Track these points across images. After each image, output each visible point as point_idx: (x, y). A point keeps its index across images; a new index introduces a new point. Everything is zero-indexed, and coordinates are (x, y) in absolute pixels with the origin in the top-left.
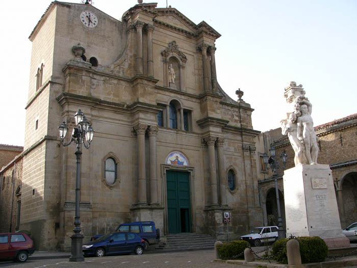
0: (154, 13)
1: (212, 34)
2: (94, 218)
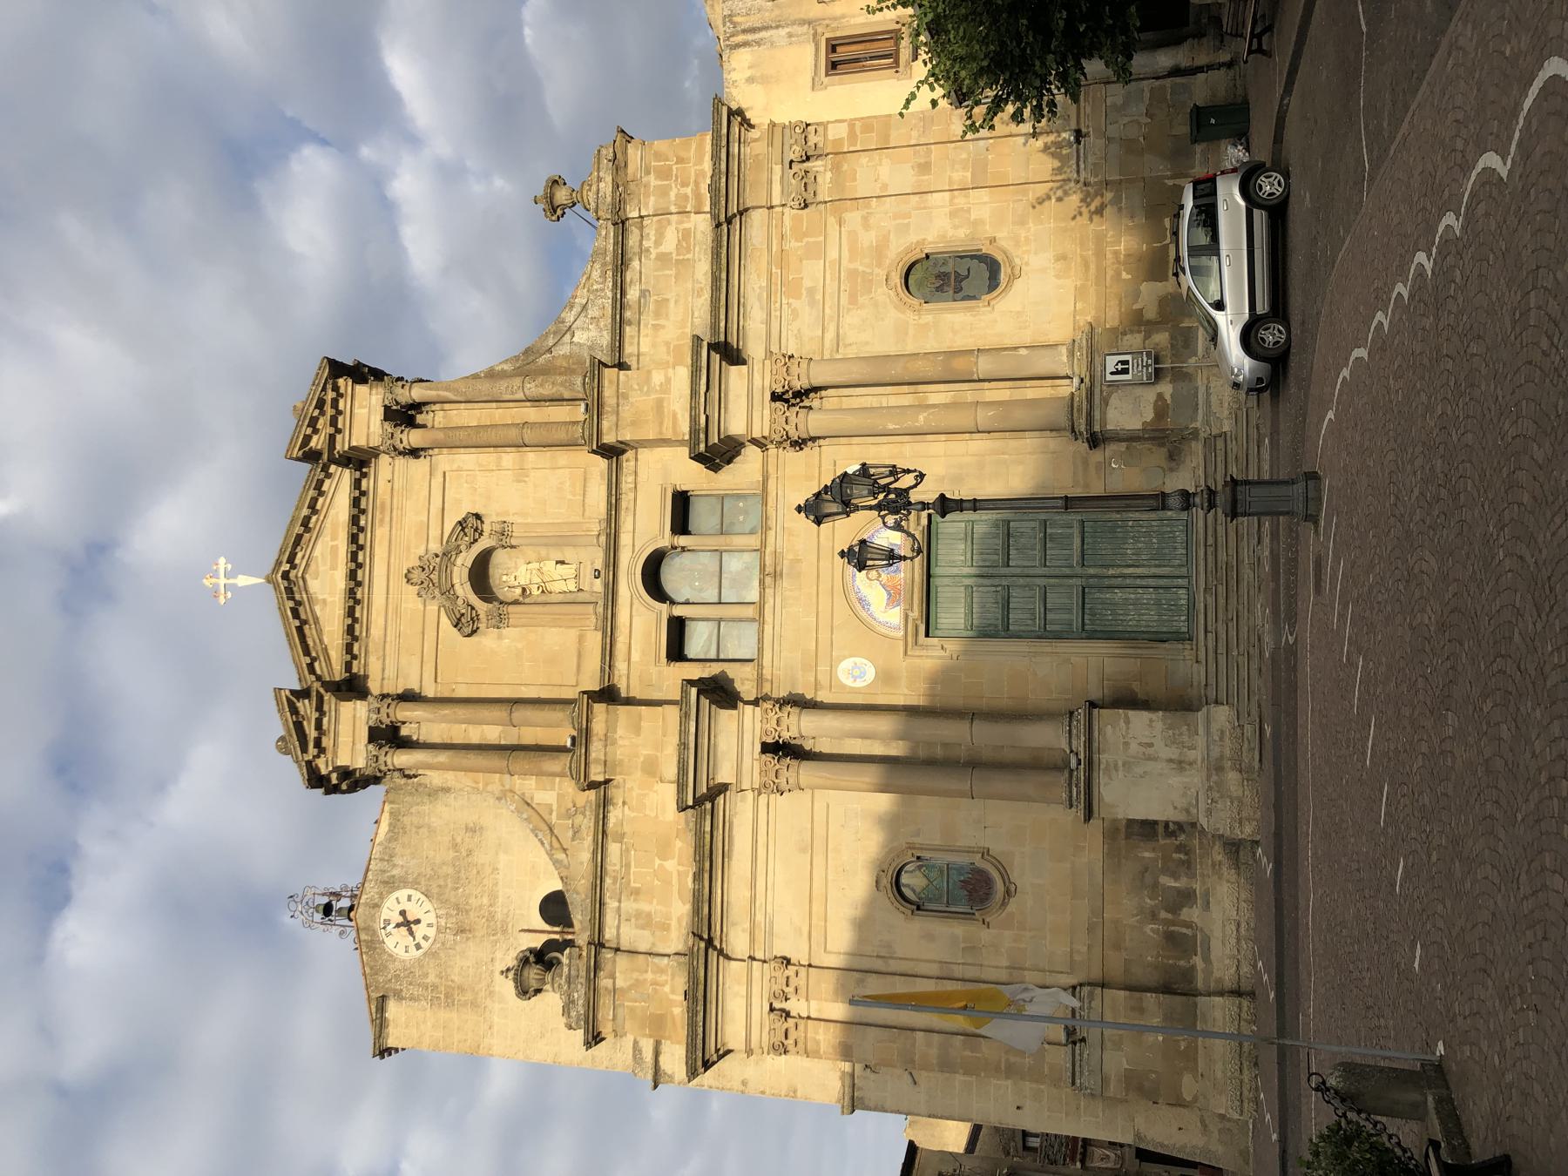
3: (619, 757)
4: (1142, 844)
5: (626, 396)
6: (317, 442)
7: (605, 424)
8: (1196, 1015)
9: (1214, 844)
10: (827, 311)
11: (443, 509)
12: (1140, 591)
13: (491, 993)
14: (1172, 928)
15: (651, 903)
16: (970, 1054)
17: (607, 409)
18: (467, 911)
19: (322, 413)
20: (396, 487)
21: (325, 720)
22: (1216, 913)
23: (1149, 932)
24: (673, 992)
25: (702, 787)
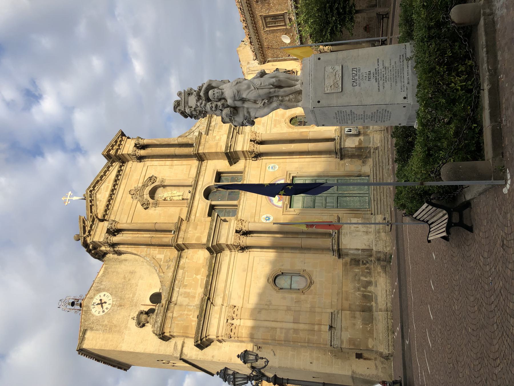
0: (93, 221)
1: (118, 143)
2: (350, 309)
3: (188, 236)
4: (355, 267)
5: (208, 142)
6: (112, 152)
7: (200, 148)
8: (373, 319)
9: (378, 266)
10: (268, 128)
11: (145, 176)
12: (354, 198)
13: (126, 327)
14: (365, 293)
15: (190, 289)
16: (295, 336)
17: (201, 144)
18: (124, 299)
19: (116, 144)
20: (132, 169)
21: (93, 226)
22: (379, 288)
23: (357, 295)
24: (193, 317)
25: (214, 243)
